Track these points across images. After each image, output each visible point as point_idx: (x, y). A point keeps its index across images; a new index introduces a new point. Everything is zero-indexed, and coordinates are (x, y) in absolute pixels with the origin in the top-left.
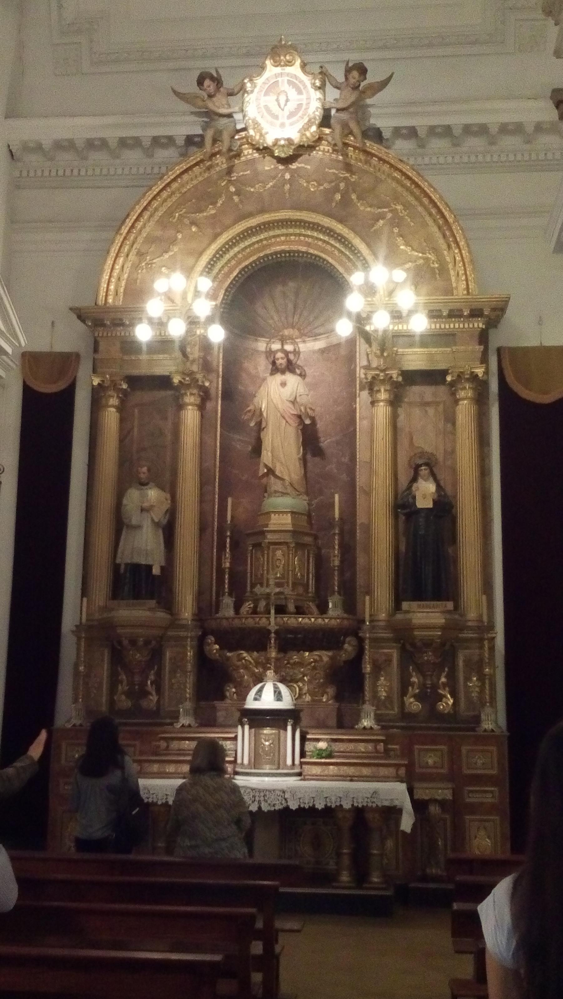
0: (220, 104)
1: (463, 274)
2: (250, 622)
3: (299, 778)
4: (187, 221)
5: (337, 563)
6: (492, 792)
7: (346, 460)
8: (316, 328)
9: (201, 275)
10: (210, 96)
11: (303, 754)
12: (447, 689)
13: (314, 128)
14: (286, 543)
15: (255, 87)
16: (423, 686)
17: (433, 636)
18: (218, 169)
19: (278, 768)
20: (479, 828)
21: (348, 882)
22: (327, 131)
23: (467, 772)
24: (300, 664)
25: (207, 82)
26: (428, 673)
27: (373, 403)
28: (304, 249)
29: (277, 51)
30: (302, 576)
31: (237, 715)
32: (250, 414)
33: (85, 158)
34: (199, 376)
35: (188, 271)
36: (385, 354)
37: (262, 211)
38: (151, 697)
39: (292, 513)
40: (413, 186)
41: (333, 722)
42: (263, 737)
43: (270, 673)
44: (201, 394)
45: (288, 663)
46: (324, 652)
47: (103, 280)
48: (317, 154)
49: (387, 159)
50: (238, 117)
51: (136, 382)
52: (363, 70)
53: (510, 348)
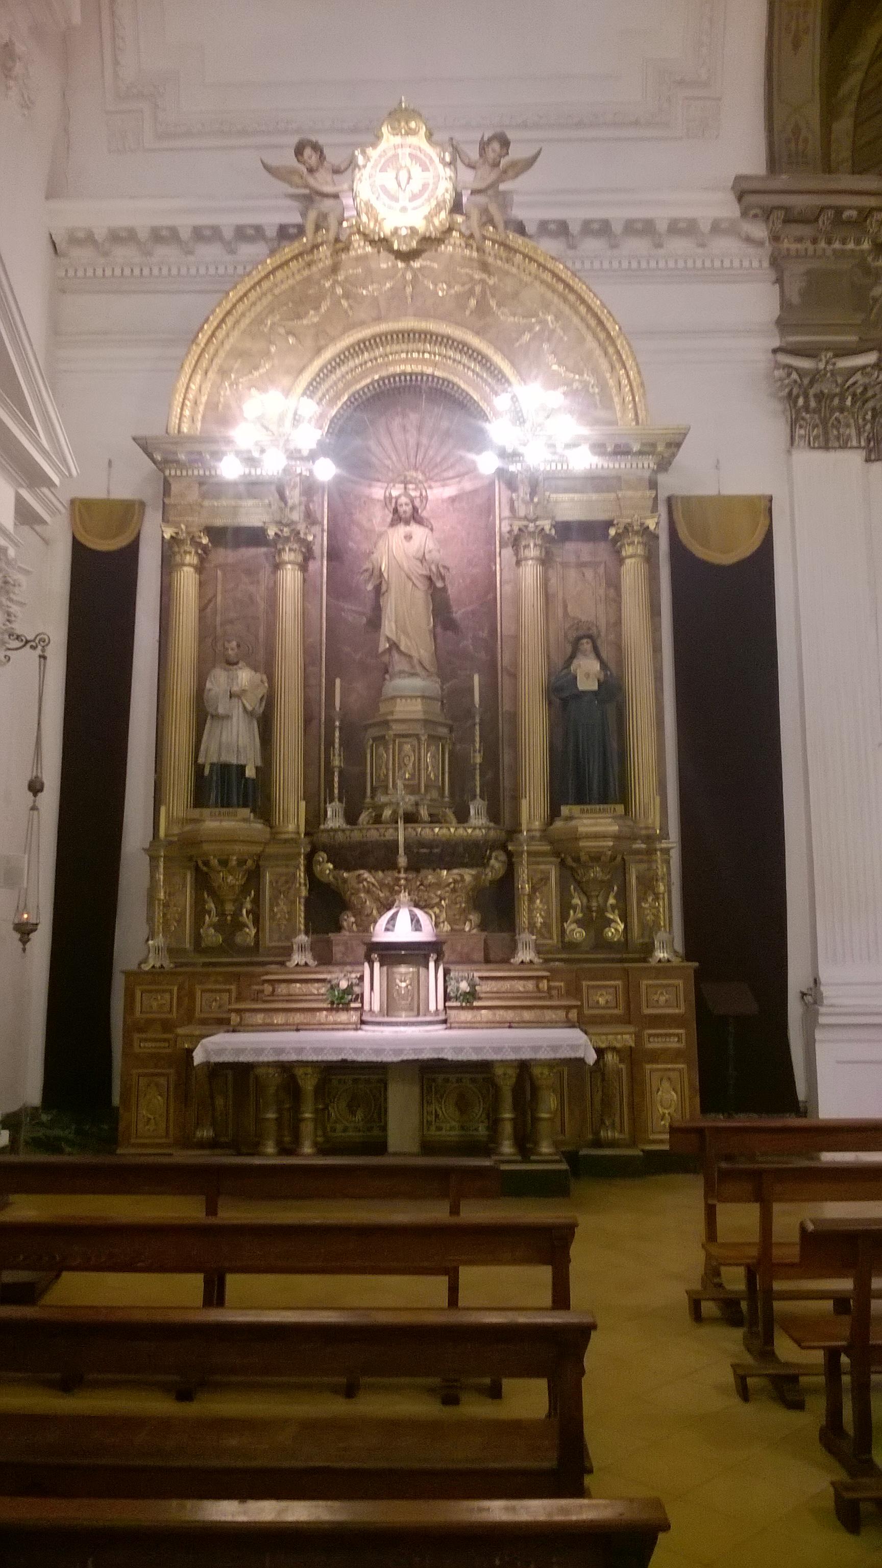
0: (323, 182)
1: (629, 403)
2: (373, 834)
3: (444, 1026)
4: (282, 331)
5: (478, 760)
6: (677, 1035)
7: (484, 634)
8: (445, 470)
9: (304, 394)
10: (311, 170)
11: (447, 998)
12: (616, 912)
13: (443, 215)
14: (417, 736)
15: (369, 160)
16: (588, 909)
17: (603, 847)
18: (321, 265)
19: (418, 1015)
20: (661, 1080)
21: (511, 1155)
22: (460, 219)
23: (647, 1011)
24: (439, 885)
25: (308, 152)
26: (593, 893)
27: (518, 563)
28: (429, 370)
29: (398, 116)
30: (436, 777)
31: (361, 951)
32: (367, 575)
33: (149, 254)
34: (302, 527)
35: (287, 392)
36: (536, 500)
37: (378, 319)
38: (247, 930)
39: (423, 697)
40: (567, 290)
41: (479, 955)
42: (398, 976)
43: (404, 896)
44: (304, 550)
45: (421, 884)
46: (467, 870)
47: (176, 403)
48: (447, 249)
49: (535, 256)
50: (347, 201)
51: (218, 535)
52: (505, 143)
53: (683, 498)
